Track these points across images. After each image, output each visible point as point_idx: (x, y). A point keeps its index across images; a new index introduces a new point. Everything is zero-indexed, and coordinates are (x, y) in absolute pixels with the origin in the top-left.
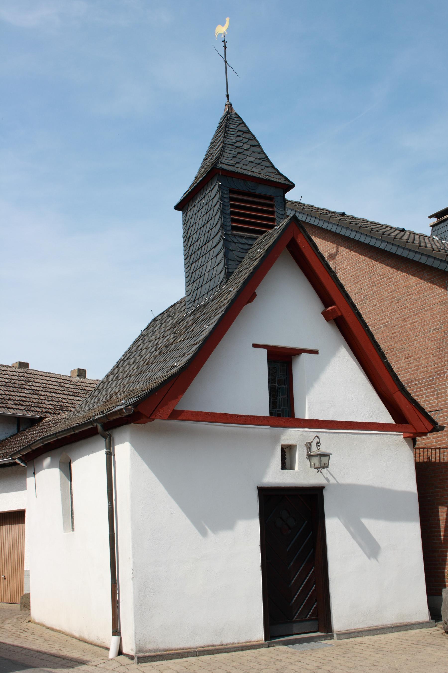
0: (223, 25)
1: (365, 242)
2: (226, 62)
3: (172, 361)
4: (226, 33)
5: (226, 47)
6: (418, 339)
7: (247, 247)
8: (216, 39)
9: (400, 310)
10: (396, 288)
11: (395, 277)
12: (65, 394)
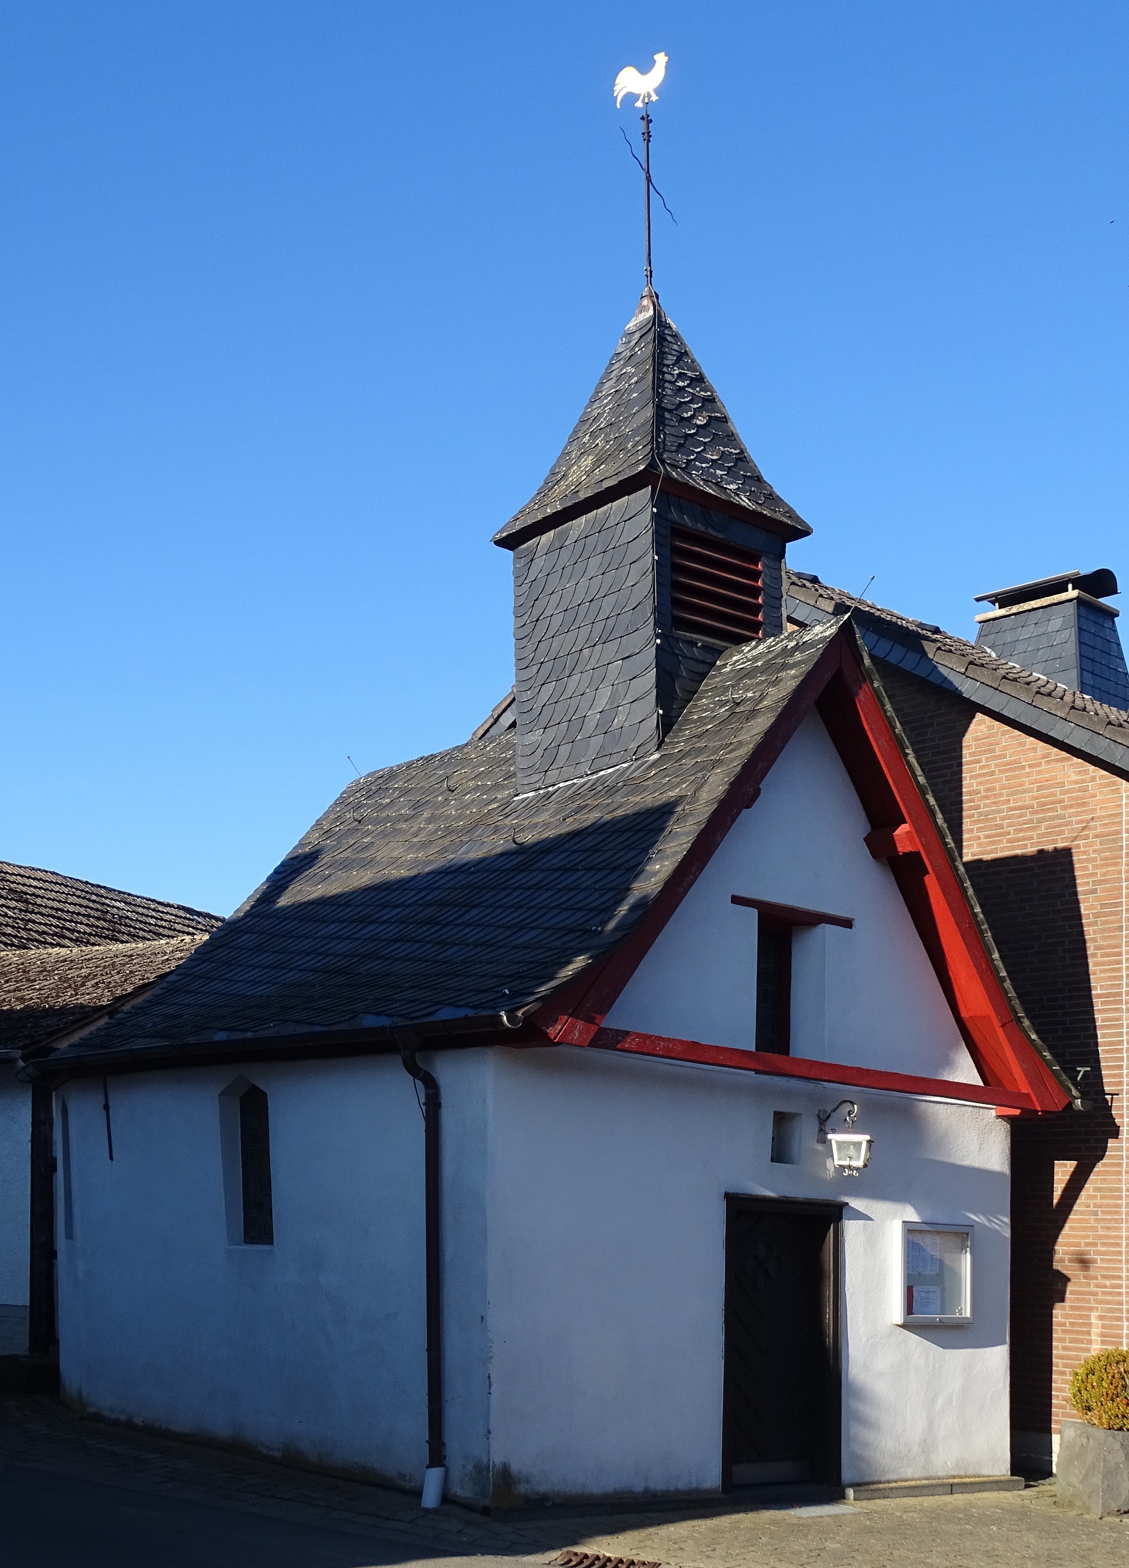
0: (645, 67)
1: (916, 672)
2: (649, 179)
3: (464, 895)
4: (654, 98)
6: (1027, 907)
7: (701, 668)
9: (987, 837)
10: (982, 788)
11: (984, 763)
12: (43, 915)
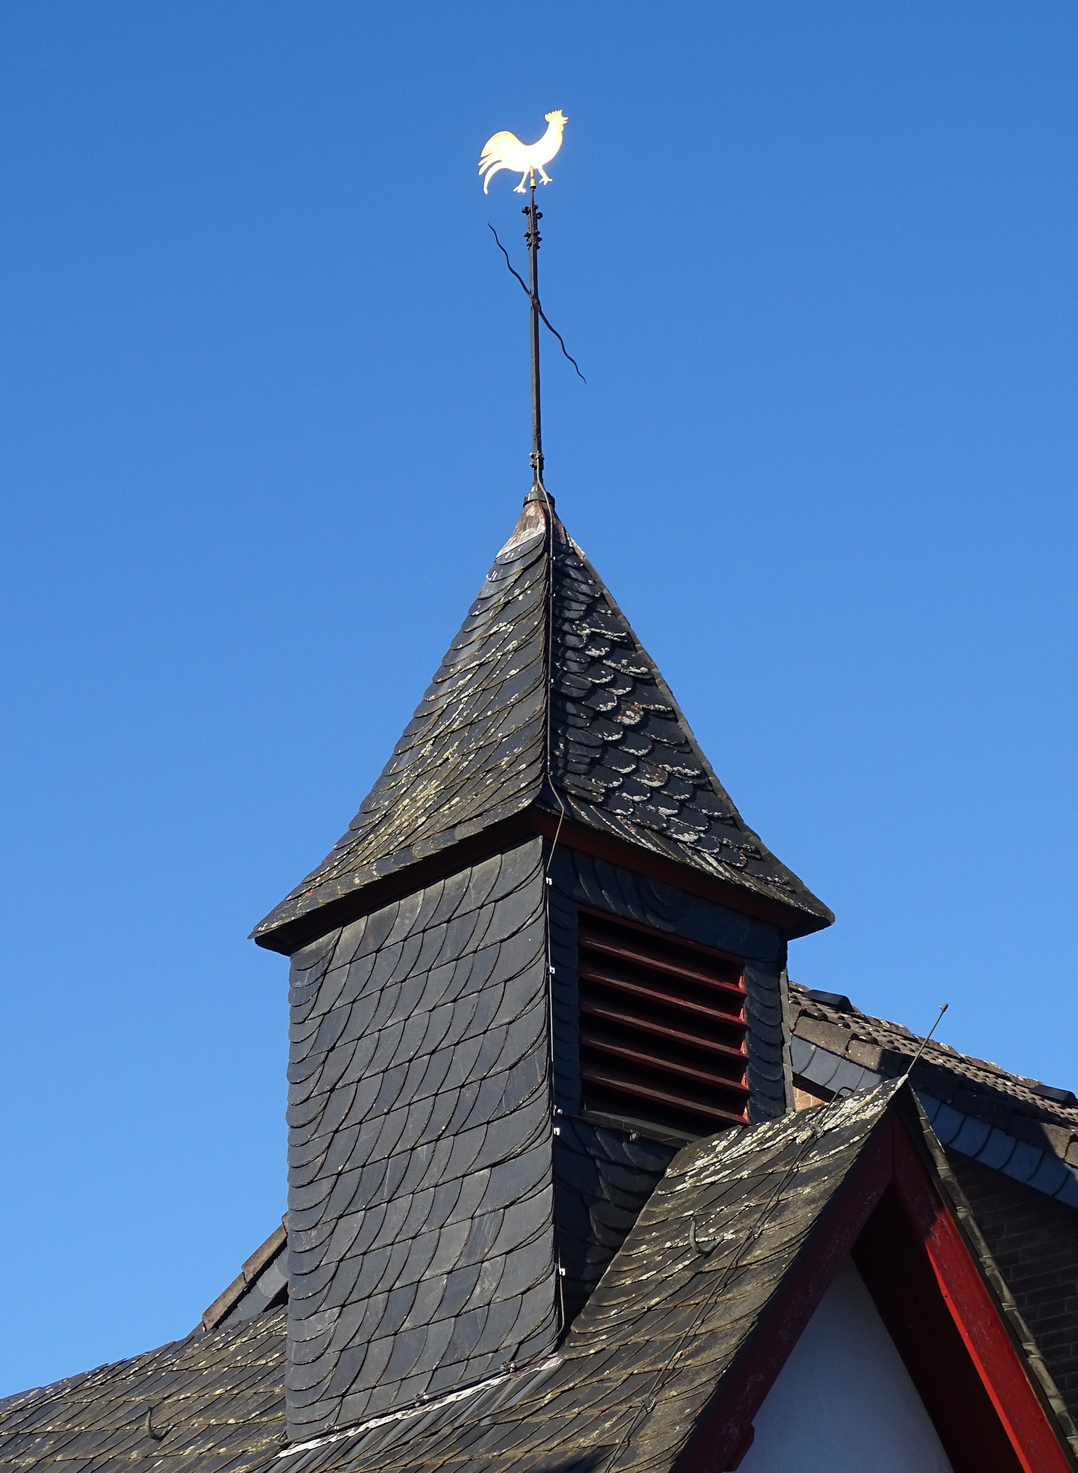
2: (537, 308)
5: (540, 239)
7: (638, 1183)
8: (486, 192)
